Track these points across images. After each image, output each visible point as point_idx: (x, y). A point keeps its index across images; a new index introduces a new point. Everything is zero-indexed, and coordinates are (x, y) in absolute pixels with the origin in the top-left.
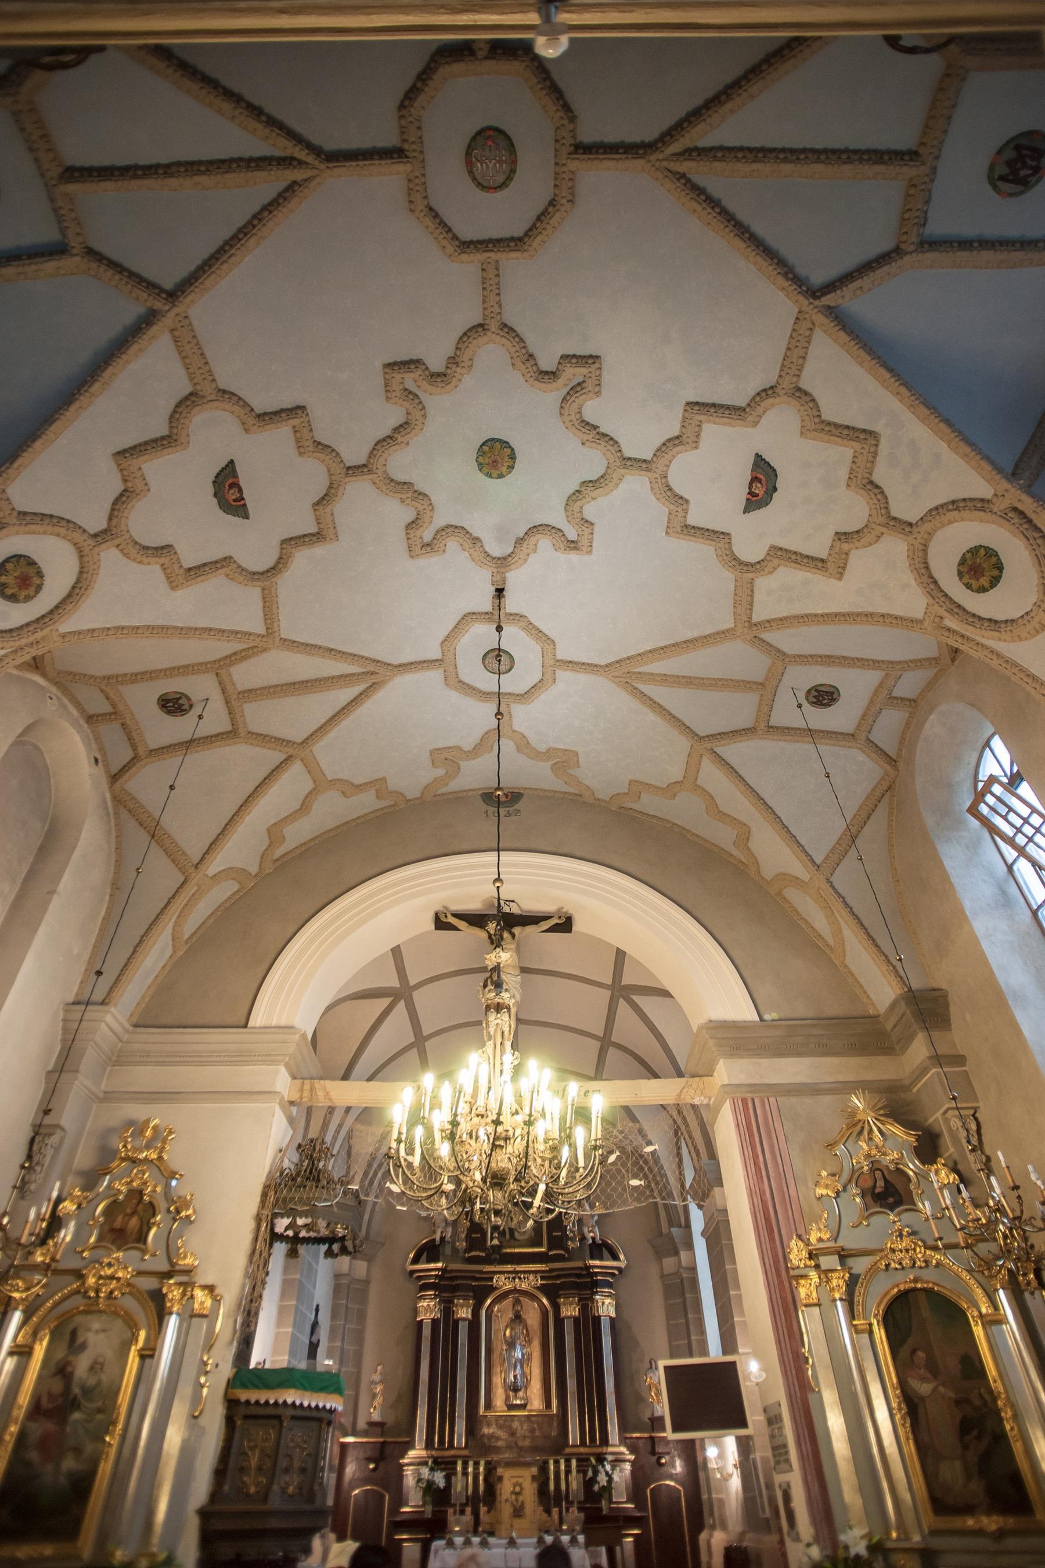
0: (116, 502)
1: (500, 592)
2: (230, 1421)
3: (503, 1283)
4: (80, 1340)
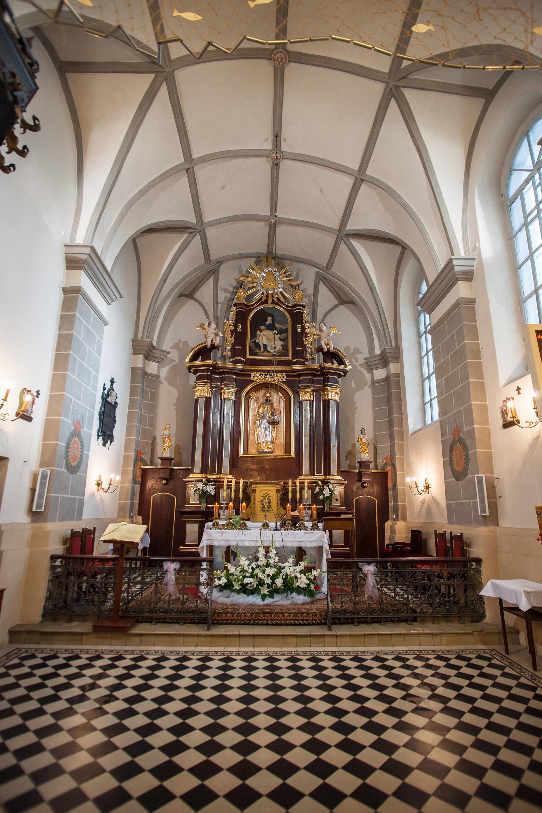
3: (257, 377)
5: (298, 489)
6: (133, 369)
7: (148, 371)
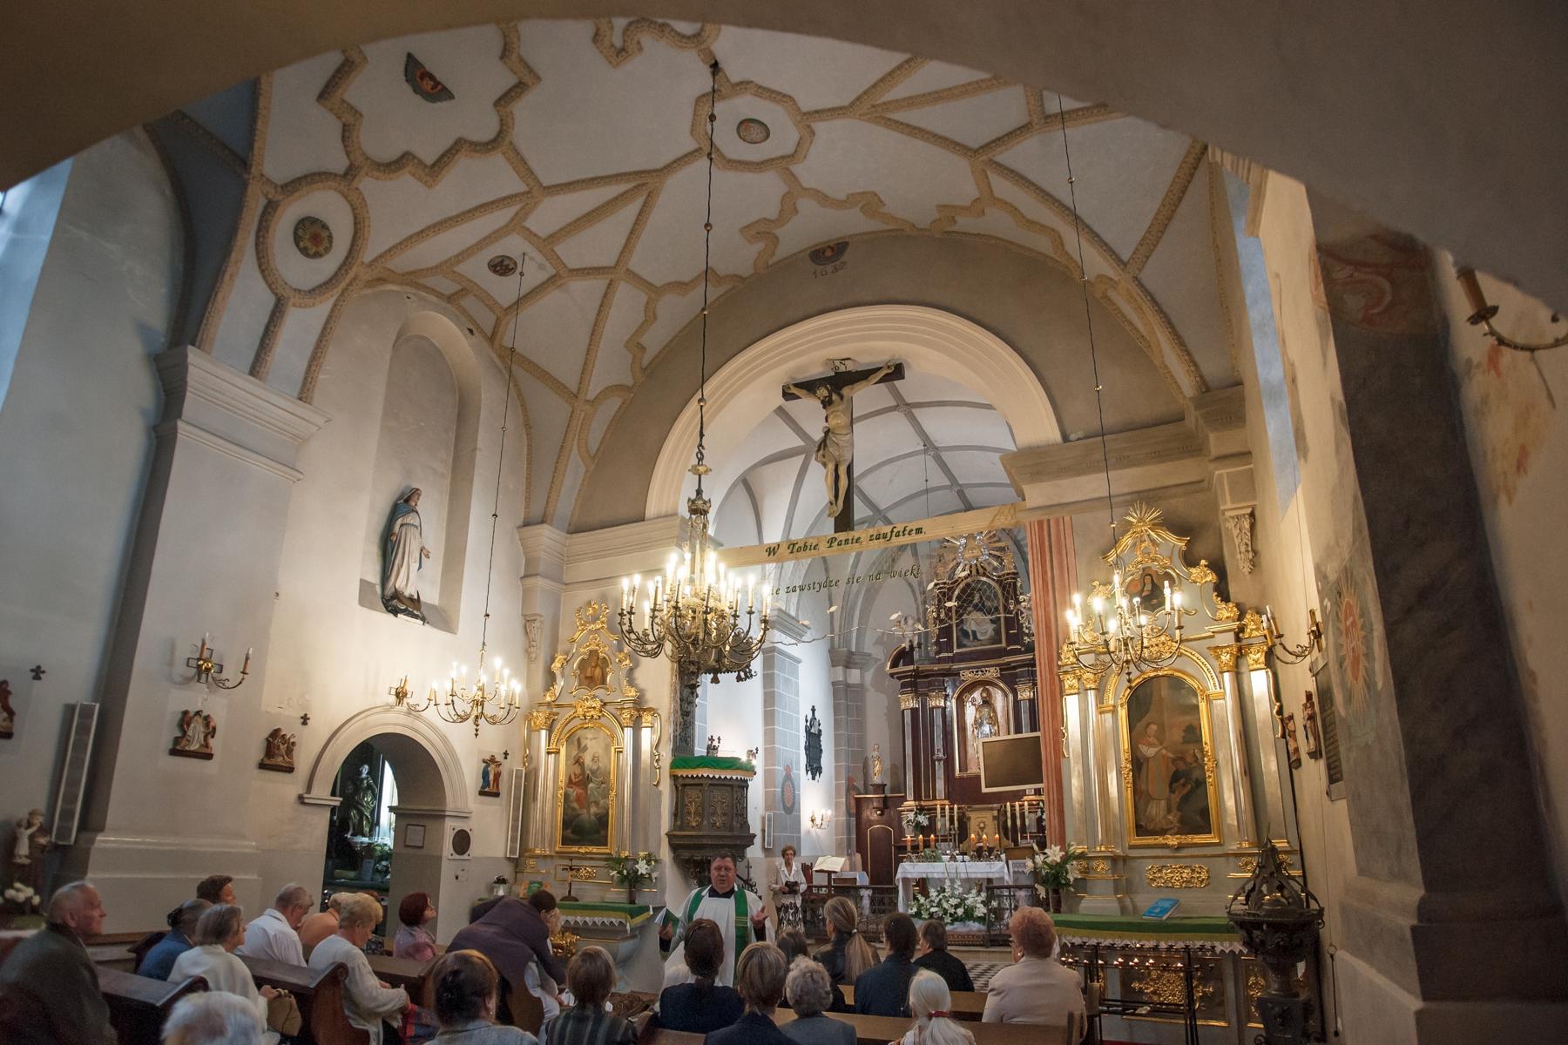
0: (344, 139)
1: (715, 67)
6: (833, 684)
7: (850, 681)
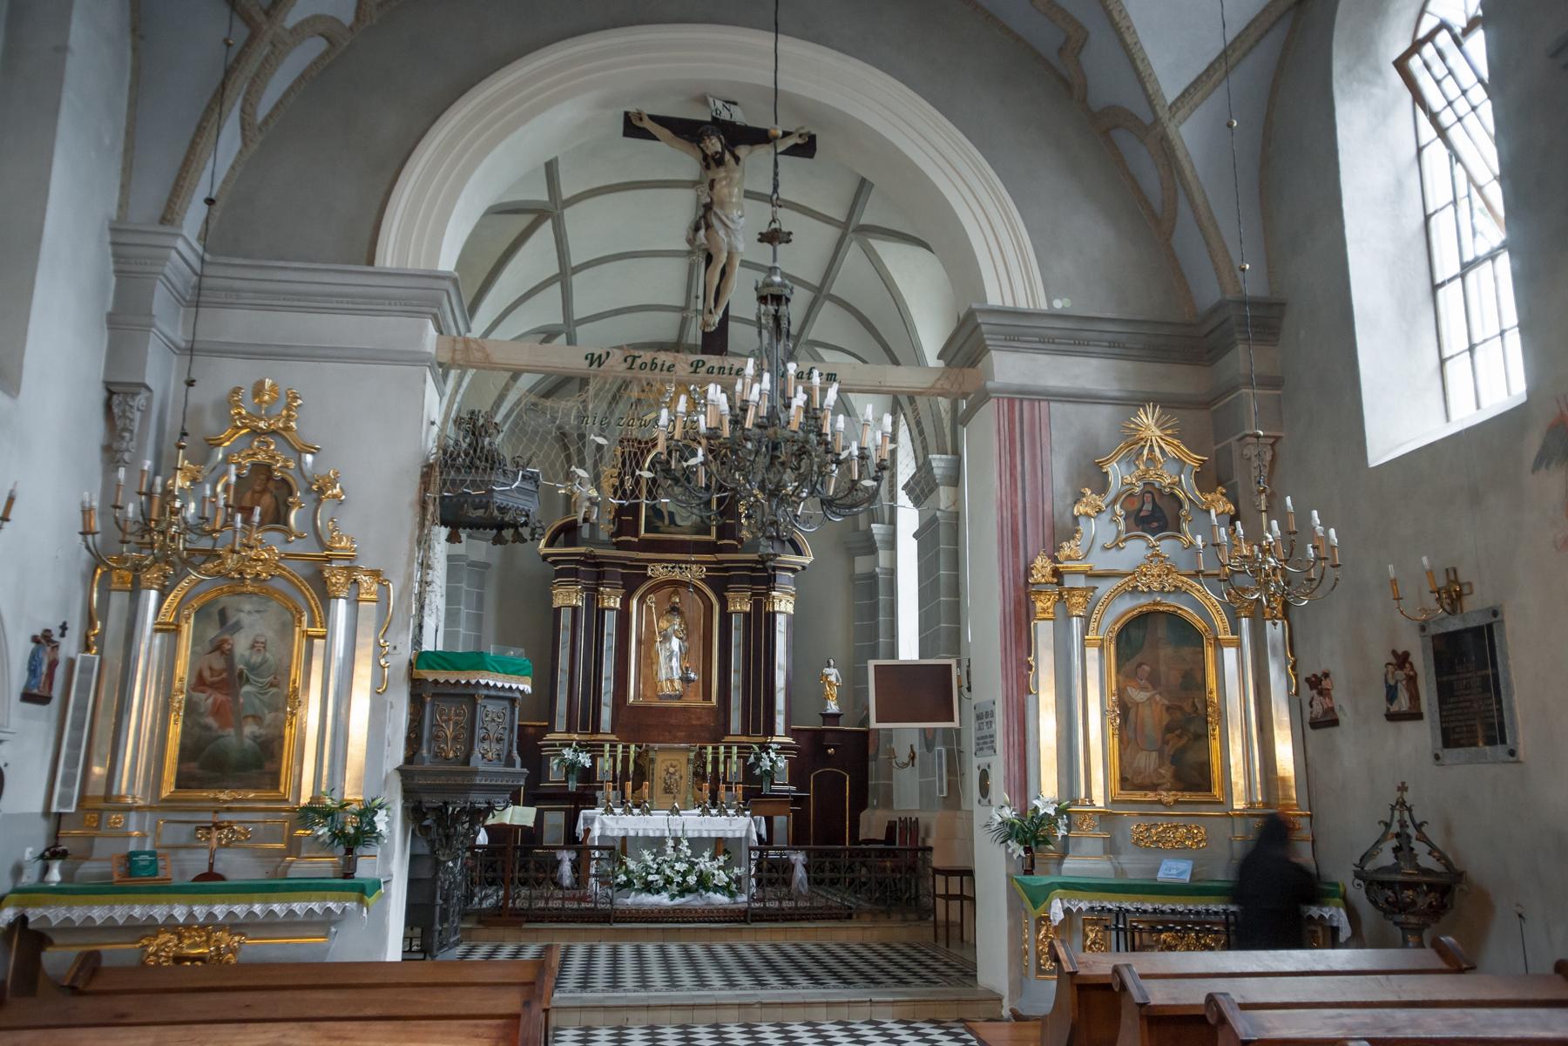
2: (416, 701)
3: (658, 572)
4: (232, 621)
5: (722, 758)
